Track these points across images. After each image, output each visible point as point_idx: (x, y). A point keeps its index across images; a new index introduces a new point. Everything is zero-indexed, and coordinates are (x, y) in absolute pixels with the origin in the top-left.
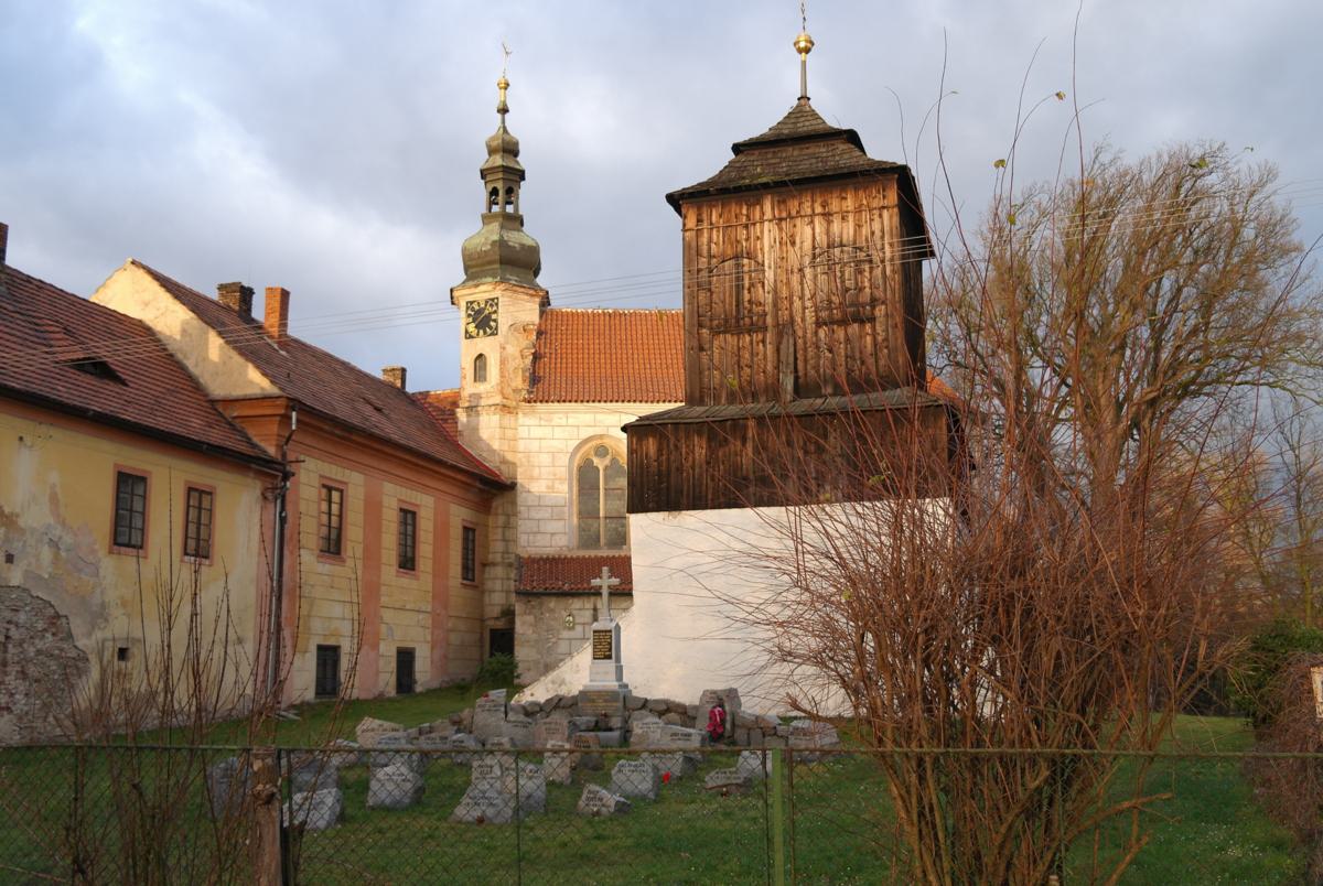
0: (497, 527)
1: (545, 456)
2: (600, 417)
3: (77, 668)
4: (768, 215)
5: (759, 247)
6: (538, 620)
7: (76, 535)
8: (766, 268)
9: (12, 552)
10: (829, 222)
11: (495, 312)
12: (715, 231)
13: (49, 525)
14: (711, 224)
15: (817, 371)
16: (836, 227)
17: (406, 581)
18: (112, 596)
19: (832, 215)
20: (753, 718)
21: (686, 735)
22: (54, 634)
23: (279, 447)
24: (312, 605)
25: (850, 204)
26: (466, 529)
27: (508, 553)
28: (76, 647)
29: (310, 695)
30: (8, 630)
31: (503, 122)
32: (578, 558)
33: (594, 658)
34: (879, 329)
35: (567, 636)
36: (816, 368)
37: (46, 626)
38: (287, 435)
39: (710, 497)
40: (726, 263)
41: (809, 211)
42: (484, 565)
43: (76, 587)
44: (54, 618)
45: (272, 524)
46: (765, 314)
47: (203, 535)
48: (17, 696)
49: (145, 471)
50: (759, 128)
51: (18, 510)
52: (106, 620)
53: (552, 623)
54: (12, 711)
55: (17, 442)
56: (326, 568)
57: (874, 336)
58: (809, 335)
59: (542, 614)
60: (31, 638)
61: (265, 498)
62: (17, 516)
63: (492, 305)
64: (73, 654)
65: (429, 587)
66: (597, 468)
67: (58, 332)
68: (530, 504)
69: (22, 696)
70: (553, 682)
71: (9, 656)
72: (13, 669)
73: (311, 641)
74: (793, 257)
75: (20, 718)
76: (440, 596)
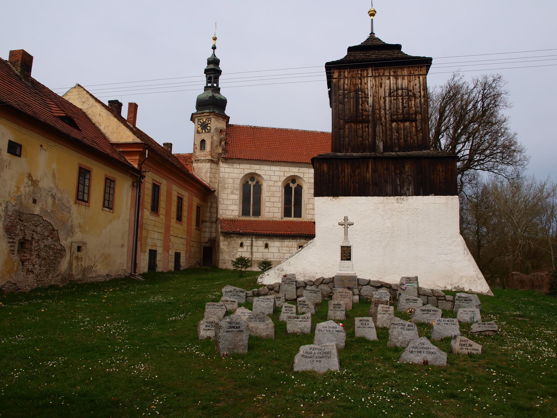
0: (208, 207)
1: (231, 179)
2: (291, 168)
3: (61, 254)
4: (370, 74)
5: (366, 87)
6: (229, 244)
7: (62, 193)
8: (369, 97)
9: (36, 199)
10: (397, 79)
11: (210, 123)
12: (346, 80)
13: (51, 188)
14: (345, 76)
15: (391, 141)
16: (400, 81)
17: (178, 226)
18: (76, 222)
19: (398, 76)
20: (430, 291)
21: (414, 300)
22: (52, 238)
23: (139, 165)
24: (148, 232)
25: (405, 72)
26: (197, 207)
27: (211, 217)
28: (60, 244)
29: (146, 270)
30: (33, 235)
31: (214, 52)
32: (242, 220)
33: (341, 260)
34: (419, 125)
35: (241, 251)
36: (391, 139)
37: (48, 234)
38: (142, 161)
39: (352, 190)
40: (351, 93)
41: (388, 74)
42: (202, 222)
43: (61, 217)
44: (52, 230)
45: (135, 197)
46: (369, 115)
47: (111, 199)
48: (36, 266)
49: (91, 168)
50: (358, 43)
51: (39, 179)
52: (73, 233)
53: (235, 245)
54: (34, 273)
55: (40, 147)
56: (153, 218)
57: (416, 127)
58: (388, 126)
59: (231, 241)
60: (42, 239)
61: (133, 186)
62: (38, 182)
63: (208, 121)
64: (59, 247)
65: (186, 229)
66: (291, 188)
67: (53, 105)
68: (224, 198)
69: (38, 266)
70: (278, 270)
71: (33, 247)
72: (35, 253)
73: (147, 248)
74: (382, 92)
75: (37, 276)
76: (188, 232)
